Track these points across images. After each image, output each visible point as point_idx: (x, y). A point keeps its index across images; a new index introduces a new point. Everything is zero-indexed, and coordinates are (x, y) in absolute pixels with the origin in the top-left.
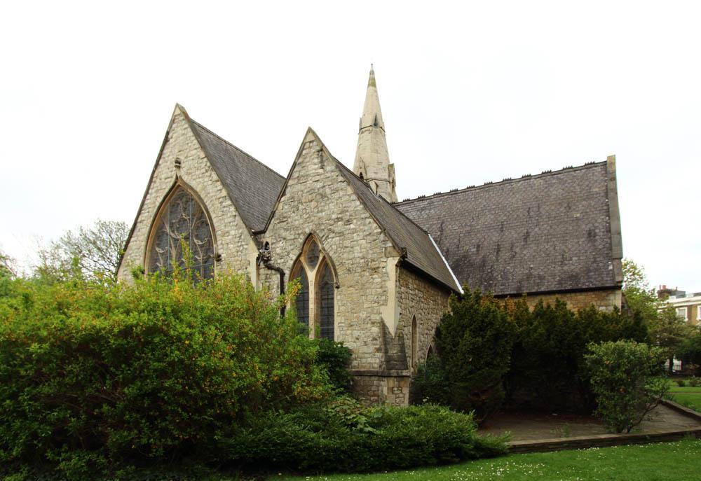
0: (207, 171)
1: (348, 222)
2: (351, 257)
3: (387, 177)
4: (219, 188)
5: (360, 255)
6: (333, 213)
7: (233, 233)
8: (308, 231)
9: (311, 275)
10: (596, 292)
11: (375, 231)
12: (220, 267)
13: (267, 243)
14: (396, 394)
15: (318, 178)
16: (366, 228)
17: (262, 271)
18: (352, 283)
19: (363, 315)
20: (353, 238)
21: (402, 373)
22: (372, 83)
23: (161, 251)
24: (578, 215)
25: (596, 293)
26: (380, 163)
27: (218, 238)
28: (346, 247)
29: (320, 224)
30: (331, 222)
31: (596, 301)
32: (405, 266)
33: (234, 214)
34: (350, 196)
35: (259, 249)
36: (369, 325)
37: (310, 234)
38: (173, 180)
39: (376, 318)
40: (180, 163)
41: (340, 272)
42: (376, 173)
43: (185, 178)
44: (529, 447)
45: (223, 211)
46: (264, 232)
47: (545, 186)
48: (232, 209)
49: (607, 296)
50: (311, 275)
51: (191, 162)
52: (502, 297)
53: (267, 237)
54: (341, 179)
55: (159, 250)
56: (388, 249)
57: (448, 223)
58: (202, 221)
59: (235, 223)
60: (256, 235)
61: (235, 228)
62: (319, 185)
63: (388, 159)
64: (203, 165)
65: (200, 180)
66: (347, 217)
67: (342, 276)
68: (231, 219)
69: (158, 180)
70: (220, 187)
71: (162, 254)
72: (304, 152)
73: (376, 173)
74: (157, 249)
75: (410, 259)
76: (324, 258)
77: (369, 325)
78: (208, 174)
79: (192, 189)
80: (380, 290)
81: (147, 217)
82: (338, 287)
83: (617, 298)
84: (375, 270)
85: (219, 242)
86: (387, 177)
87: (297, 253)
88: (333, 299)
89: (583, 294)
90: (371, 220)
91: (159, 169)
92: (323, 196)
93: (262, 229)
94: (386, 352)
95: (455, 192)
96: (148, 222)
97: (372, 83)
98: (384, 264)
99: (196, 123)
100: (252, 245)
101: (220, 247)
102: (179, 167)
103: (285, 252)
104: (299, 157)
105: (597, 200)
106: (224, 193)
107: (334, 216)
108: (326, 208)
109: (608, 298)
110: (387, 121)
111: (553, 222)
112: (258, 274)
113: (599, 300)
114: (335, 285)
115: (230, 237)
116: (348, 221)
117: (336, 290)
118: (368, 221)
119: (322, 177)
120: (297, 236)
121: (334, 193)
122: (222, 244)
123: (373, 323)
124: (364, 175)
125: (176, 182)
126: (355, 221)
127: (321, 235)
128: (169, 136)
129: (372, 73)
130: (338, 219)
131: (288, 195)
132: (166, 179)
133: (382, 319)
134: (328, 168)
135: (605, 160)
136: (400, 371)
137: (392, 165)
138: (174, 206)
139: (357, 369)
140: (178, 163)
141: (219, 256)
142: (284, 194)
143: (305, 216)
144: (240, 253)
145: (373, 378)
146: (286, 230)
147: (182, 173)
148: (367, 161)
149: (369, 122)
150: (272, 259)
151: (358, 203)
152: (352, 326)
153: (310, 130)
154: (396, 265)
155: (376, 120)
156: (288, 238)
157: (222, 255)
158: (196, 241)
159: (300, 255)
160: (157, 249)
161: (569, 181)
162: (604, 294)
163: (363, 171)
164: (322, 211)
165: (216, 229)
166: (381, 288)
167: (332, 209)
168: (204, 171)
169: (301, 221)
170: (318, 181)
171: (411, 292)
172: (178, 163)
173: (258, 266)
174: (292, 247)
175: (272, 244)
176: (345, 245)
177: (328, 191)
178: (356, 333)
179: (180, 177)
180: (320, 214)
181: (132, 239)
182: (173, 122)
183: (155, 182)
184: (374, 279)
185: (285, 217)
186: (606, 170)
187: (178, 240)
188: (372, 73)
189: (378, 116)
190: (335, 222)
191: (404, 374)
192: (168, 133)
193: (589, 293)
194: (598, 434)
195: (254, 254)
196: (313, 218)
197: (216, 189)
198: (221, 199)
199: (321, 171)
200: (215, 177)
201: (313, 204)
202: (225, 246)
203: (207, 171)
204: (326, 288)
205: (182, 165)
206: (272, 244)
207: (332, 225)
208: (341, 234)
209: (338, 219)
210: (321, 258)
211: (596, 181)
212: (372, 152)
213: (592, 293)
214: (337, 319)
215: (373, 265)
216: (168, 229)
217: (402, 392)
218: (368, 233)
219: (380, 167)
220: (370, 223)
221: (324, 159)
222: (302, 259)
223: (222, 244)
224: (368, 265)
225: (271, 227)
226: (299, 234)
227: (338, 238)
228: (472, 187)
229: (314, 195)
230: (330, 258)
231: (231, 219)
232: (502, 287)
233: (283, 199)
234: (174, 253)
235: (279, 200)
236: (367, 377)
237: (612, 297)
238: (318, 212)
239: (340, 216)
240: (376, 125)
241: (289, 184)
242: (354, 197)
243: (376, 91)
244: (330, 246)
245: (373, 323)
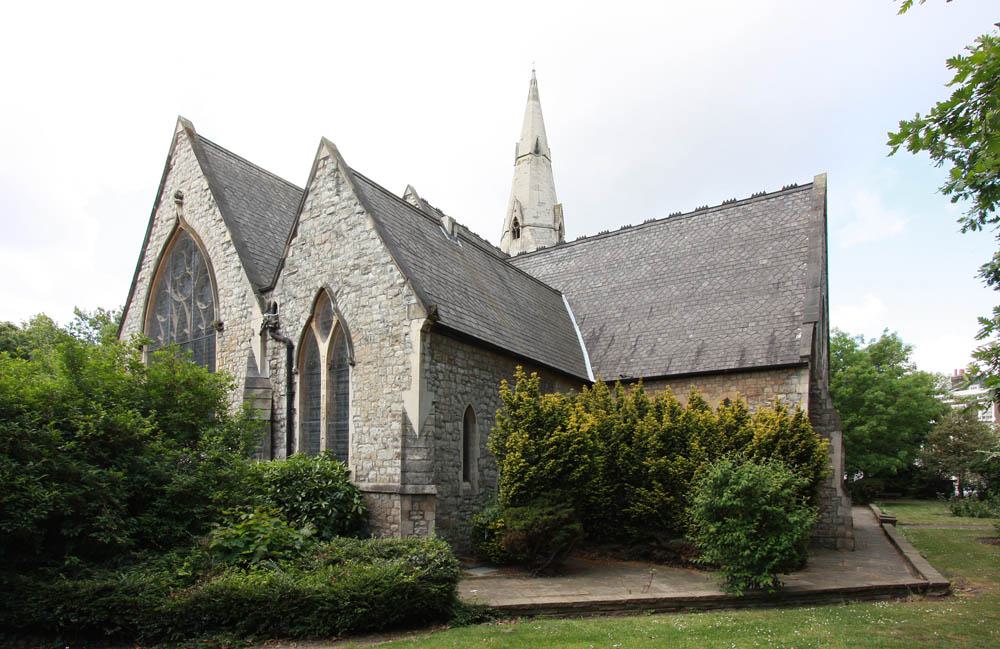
0: (211, 207)
1: (366, 271)
2: (369, 321)
3: (551, 223)
4: (222, 230)
5: (379, 317)
6: (349, 258)
7: (236, 291)
8: (320, 285)
9: (323, 347)
10: (771, 373)
11: (398, 282)
12: (222, 339)
13: (275, 305)
14: (415, 521)
15: (332, 209)
16: (387, 277)
17: (270, 344)
18: (370, 358)
19: (383, 404)
20: (371, 293)
21: (423, 489)
22: (535, 96)
23: (163, 320)
24: (765, 262)
25: (773, 373)
26: (541, 204)
27: (221, 299)
28: (364, 306)
29: (333, 276)
30: (348, 271)
31: (772, 386)
32: (437, 333)
33: (238, 264)
34: (368, 232)
35: (263, 313)
36: (389, 419)
37: (322, 289)
38: (173, 222)
39: (396, 407)
40: (181, 198)
41: (356, 342)
42: (536, 217)
43: (188, 218)
44: (680, 602)
45: (226, 262)
46: (271, 289)
47: (726, 221)
48: (237, 257)
49: (788, 378)
50: (323, 347)
51: (194, 196)
52: (627, 382)
53: (275, 297)
54: (359, 208)
55: (161, 319)
56: (413, 306)
57: (590, 279)
58: (206, 277)
59: (239, 278)
60: (262, 291)
61: (239, 284)
62: (335, 219)
63: (554, 198)
64: (206, 199)
65: (203, 219)
66: (363, 262)
67: (360, 351)
68: (235, 272)
69: (159, 223)
70: (224, 228)
71: (164, 324)
72: (318, 174)
73: (536, 217)
74: (159, 317)
75: (447, 319)
76: (338, 322)
77: (389, 419)
78: (211, 211)
79: (193, 231)
80: (401, 368)
81: (147, 273)
82: (353, 365)
83: (802, 381)
84: (396, 339)
85: (221, 305)
86: (551, 223)
87: (307, 315)
88: (348, 382)
89: (754, 375)
90: (394, 266)
91: (161, 209)
92: (338, 235)
93: (268, 285)
94: (403, 459)
95: (605, 235)
96: (147, 281)
97: (535, 96)
98: (405, 330)
99: (207, 142)
100: (256, 310)
101: (222, 311)
102: (180, 204)
103: (294, 316)
104: (313, 180)
105: (794, 239)
106: (228, 236)
107: (350, 263)
108: (341, 251)
109: (790, 381)
110: (554, 144)
111: (730, 272)
112: (264, 348)
113: (776, 384)
114: (348, 361)
115: (234, 297)
116: (366, 269)
117: (350, 368)
118: (390, 266)
119: (338, 207)
120: (308, 293)
121: (351, 229)
122: (224, 307)
123: (394, 416)
124: (519, 221)
125: (177, 224)
126: (374, 269)
127: (334, 291)
128: (172, 163)
129: (534, 82)
130: (356, 267)
131: (299, 235)
132: (167, 221)
133: (404, 409)
134: (345, 195)
135: (812, 181)
136: (420, 487)
137: (560, 205)
138: (177, 257)
139: (375, 484)
140: (179, 197)
141: (221, 324)
142: (295, 234)
143: (318, 264)
144: (243, 319)
145: (393, 497)
146: (296, 285)
147: (185, 211)
148: (525, 200)
149: (528, 148)
150: (281, 326)
151: (378, 242)
152: (369, 420)
153: (324, 142)
154: (422, 331)
155: (537, 145)
156: (299, 296)
157: (225, 323)
158: (199, 304)
159: (310, 321)
160: (159, 317)
161: (759, 214)
162: (784, 376)
163: (517, 214)
164: (337, 256)
165: (219, 287)
166: (404, 364)
167: (347, 252)
168: (207, 207)
169: (313, 271)
170: (333, 213)
171: (462, 371)
172: (179, 197)
173: (264, 341)
174: (303, 308)
175: (281, 305)
176: (362, 304)
177: (344, 227)
178: (374, 431)
179: (181, 217)
180: (334, 261)
181: (132, 305)
182: (175, 142)
183: (156, 226)
184: (395, 352)
185: (296, 267)
186: (812, 198)
187: (179, 303)
188: (534, 82)
189: (540, 141)
190: (351, 270)
191: (426, 491)
192: (170, 158)
193: (762, 375)
194: (590, 594)
195: (258, 319)
196: (326, 267)
197: (219, 231)
198: (225, 245)
199: (336, 199)
200: (219, 215)
201: (327, 246)
202: (228, 311)
203: (211, 207)
204: (340, 367)
205: (185, 201)
206: (281, 305)
207: (348, 276)
208: (358, 288)
209: (356, 267)
210: (334, 323)
211: (796, 213)
212: (531, 188)
213: (766, 374)
214: (352, 411)
215: (393, 330)
216: (169, 290)
217: (423, 519)
218: (389, 285)
219: (542, 209)
220: (391, 270)
221: (340, 182)
222: (313, 325)
223: (224, 307)
224: (388, 331)
225: (280, 281)
226: (310, 290)
227: (354, 294)
228: (628, 227)
229: (328, 233)
230: (344, 321)
231: (235, 272)
232: (643, 368)
233: (293, 242)
234: (175, 322)
235: (288, 243)
236: (386, 496)
237: (795, 380)
238: (332, 257)
239: (356, 262)
240: (537, 152)
241: (301, 220)
242: (374, 233)
243: (539, 107)
244: (345, 304)
245: (394, 416)
